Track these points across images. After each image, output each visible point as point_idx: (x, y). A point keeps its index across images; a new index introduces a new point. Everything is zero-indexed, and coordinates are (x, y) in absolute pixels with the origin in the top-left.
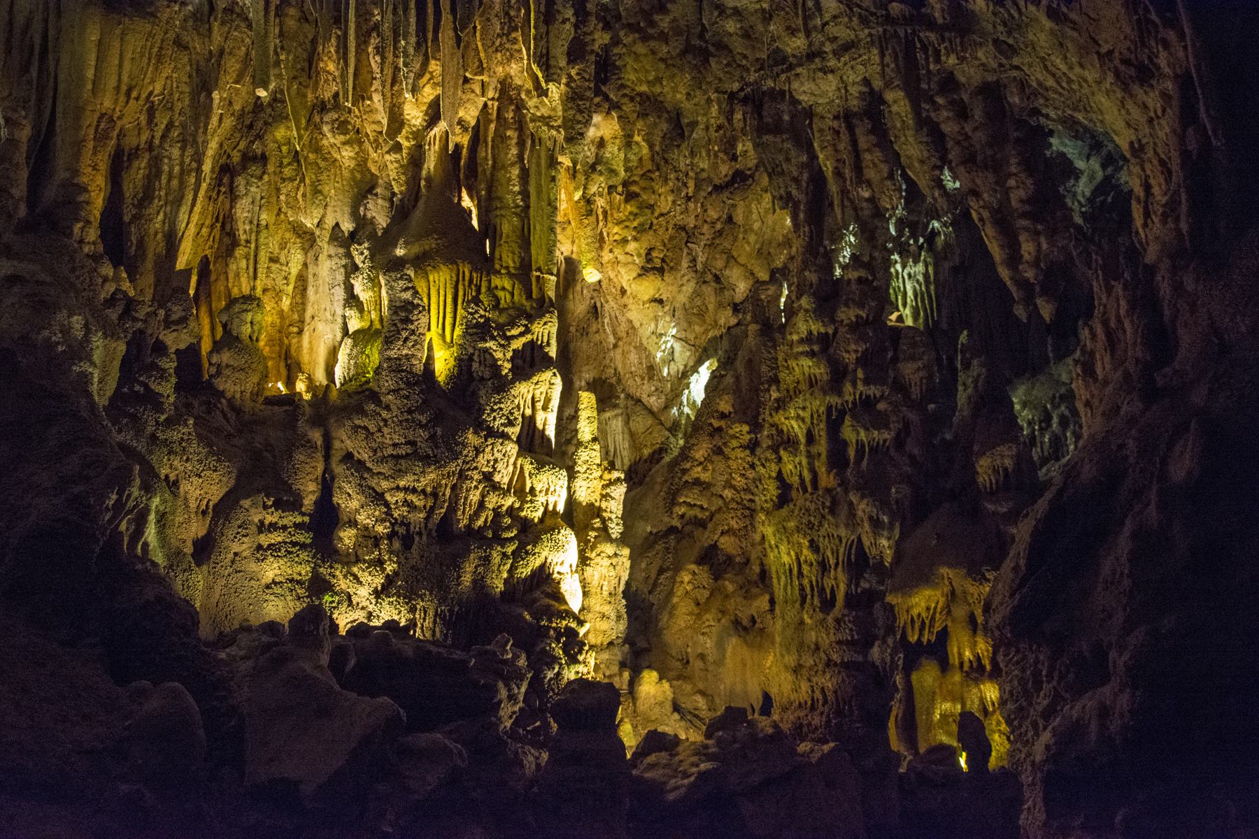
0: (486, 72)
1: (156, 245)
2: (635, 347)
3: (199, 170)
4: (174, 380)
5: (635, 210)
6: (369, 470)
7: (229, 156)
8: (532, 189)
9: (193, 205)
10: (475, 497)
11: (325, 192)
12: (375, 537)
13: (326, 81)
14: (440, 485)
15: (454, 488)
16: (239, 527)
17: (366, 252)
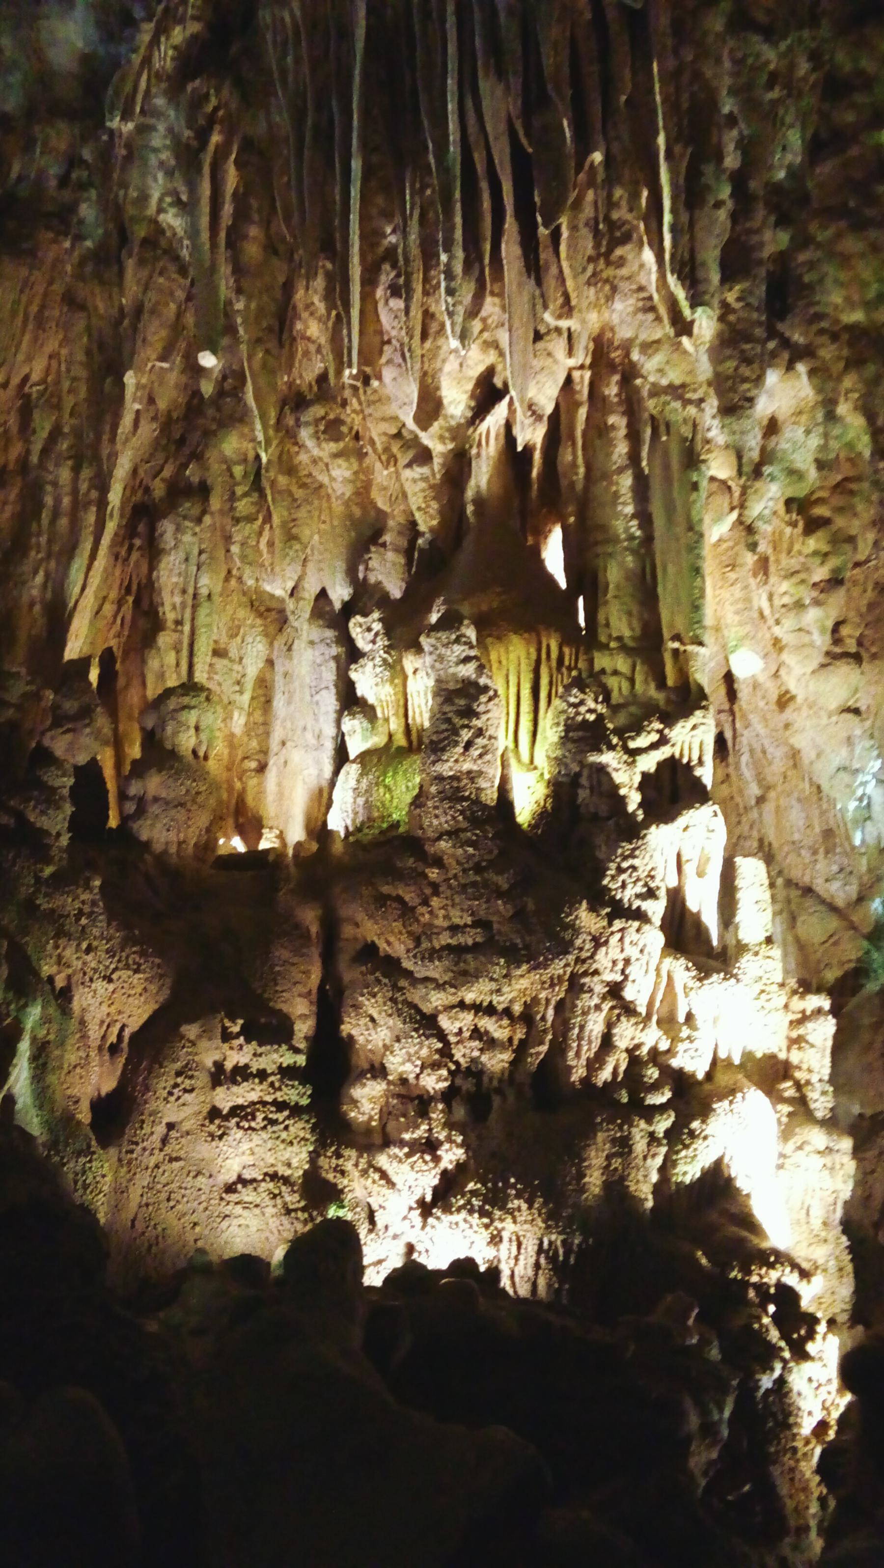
0: (575, 313)
1: (31, 623)
2: (799, 800)
3: (102, 503)
4: (69, 809)
5: (825, 548)
6: (409, 974)
7: (147, 490)
8: (657, 509)
9: (93, 557)
10: (596, 1025)
11: (305, 540)
12: (420, 1097)
13: (306, 353)
14: (535, 1000)
15: (560, 1007)
16: (178, 1074)
17: (377, 626)
